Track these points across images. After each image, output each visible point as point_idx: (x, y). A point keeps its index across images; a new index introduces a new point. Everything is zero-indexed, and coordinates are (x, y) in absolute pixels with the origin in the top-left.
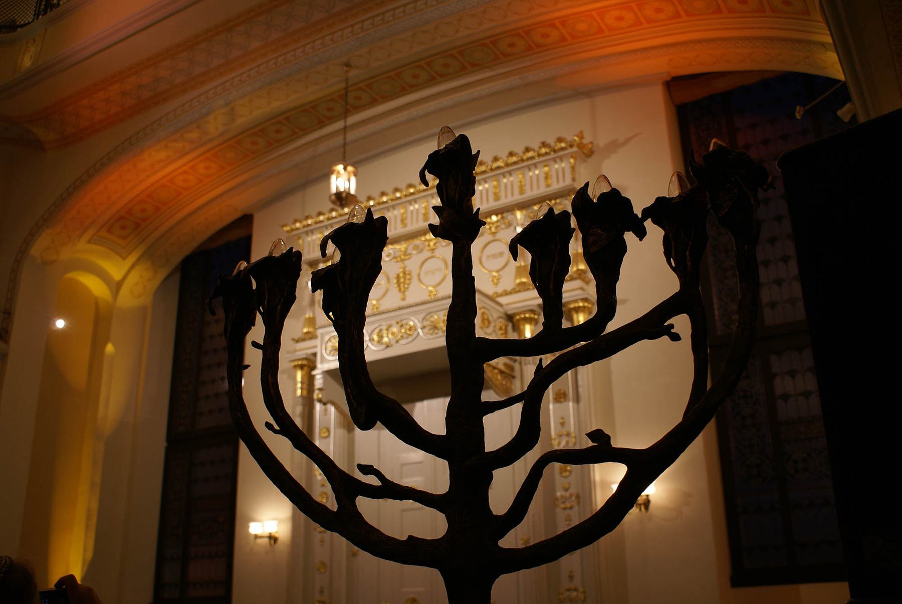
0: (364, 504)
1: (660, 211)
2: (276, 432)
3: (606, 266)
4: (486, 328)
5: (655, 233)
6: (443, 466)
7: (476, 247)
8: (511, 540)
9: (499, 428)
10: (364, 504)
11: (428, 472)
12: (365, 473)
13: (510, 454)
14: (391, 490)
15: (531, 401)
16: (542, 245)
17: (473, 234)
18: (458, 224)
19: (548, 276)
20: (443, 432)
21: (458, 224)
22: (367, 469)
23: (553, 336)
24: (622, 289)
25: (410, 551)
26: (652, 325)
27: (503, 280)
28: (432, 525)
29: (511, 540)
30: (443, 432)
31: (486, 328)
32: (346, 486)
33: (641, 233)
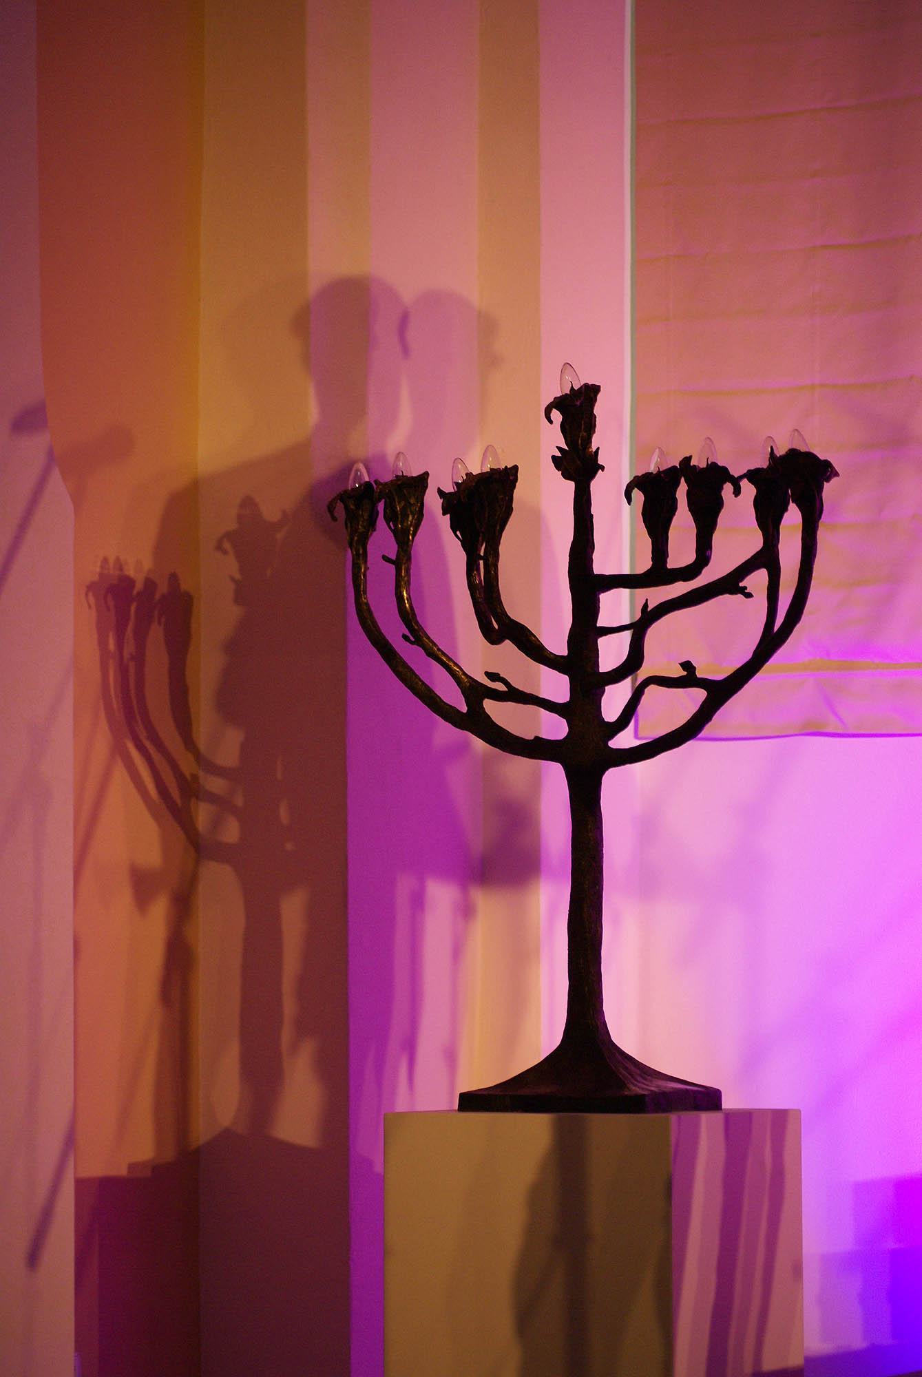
0: (489, 706)
1: (752, 476)
2: (412, 643)
3: (707, 517)
4: (602, 565)
5: (749, 490)
6: (565, 680)
7: (594, 485)
8: (624, 740)
9: (612, 652)
10: (489, 706)
11: (556, 686)
12: (493, 680)
13: (617, 675)
14: (514, 695)
15: (639, 629)
16: (655, 493)
17: (592, 475)
18: (579, 464)
19: (656, 521)
20: (565, 653)
21: (579, 464)
22: (493, 677)
23: (659, 574)
24: (718, 539)
25: (538, 749)
26: (731, 584)
27: (620, 544)
28: (555, 728)
29: (624, 740)
30: (565, 653)
31: (602, 565)
32: (475, 692)
33: (737, 492)
